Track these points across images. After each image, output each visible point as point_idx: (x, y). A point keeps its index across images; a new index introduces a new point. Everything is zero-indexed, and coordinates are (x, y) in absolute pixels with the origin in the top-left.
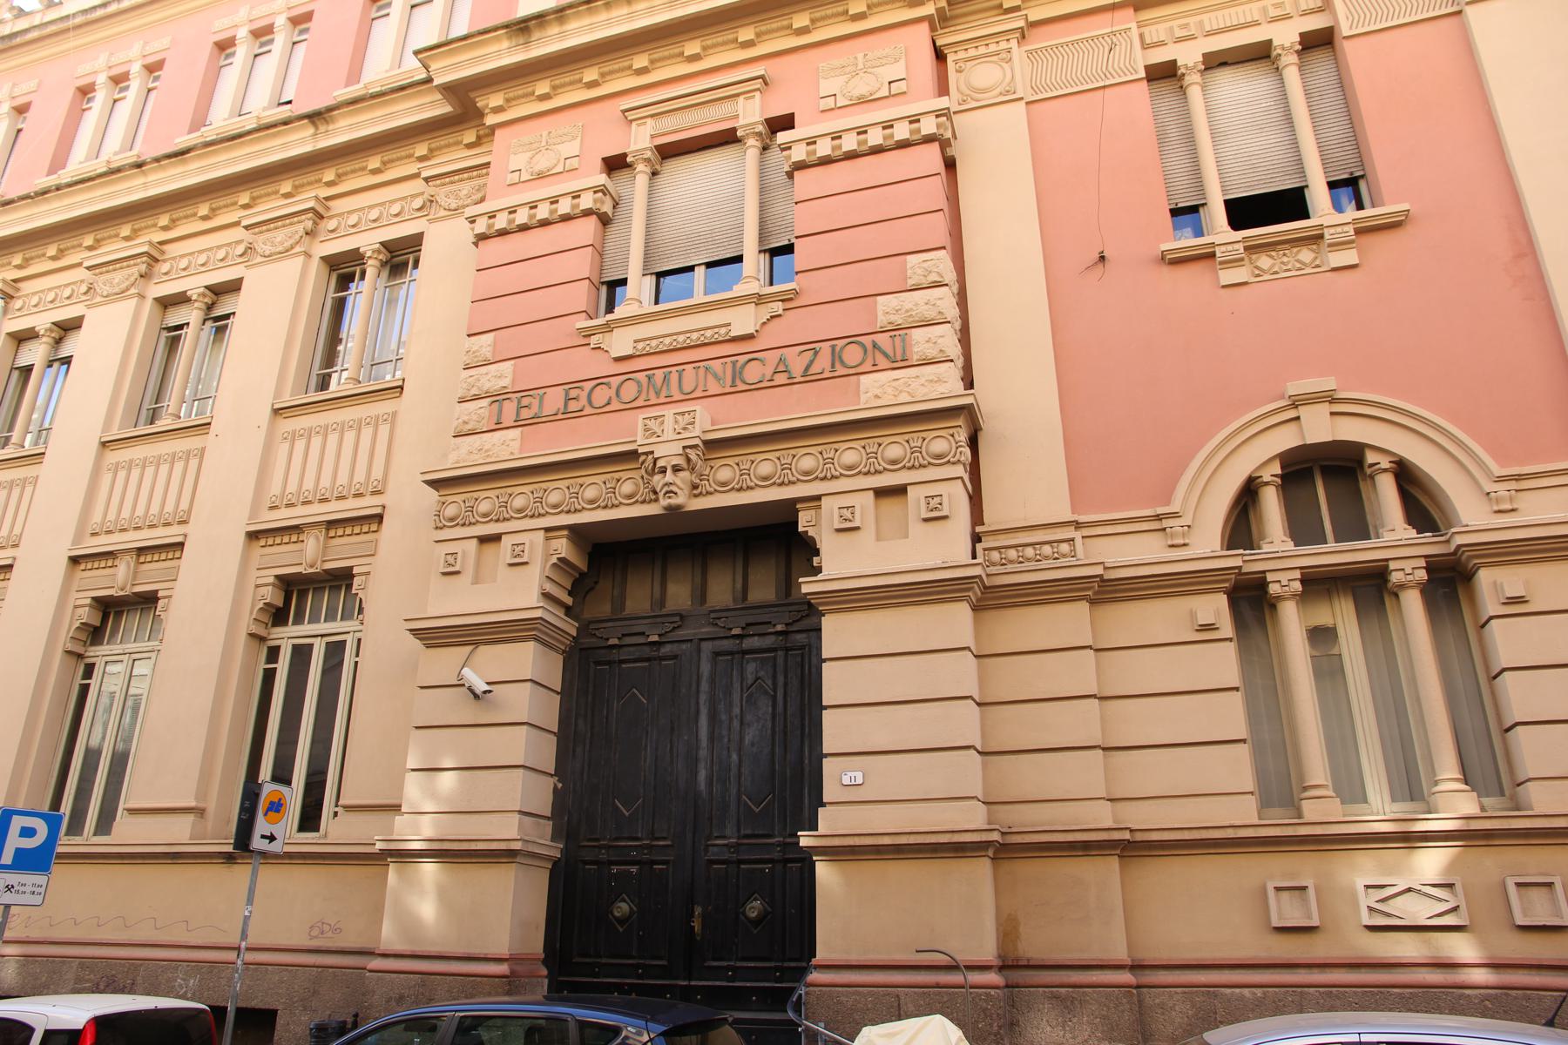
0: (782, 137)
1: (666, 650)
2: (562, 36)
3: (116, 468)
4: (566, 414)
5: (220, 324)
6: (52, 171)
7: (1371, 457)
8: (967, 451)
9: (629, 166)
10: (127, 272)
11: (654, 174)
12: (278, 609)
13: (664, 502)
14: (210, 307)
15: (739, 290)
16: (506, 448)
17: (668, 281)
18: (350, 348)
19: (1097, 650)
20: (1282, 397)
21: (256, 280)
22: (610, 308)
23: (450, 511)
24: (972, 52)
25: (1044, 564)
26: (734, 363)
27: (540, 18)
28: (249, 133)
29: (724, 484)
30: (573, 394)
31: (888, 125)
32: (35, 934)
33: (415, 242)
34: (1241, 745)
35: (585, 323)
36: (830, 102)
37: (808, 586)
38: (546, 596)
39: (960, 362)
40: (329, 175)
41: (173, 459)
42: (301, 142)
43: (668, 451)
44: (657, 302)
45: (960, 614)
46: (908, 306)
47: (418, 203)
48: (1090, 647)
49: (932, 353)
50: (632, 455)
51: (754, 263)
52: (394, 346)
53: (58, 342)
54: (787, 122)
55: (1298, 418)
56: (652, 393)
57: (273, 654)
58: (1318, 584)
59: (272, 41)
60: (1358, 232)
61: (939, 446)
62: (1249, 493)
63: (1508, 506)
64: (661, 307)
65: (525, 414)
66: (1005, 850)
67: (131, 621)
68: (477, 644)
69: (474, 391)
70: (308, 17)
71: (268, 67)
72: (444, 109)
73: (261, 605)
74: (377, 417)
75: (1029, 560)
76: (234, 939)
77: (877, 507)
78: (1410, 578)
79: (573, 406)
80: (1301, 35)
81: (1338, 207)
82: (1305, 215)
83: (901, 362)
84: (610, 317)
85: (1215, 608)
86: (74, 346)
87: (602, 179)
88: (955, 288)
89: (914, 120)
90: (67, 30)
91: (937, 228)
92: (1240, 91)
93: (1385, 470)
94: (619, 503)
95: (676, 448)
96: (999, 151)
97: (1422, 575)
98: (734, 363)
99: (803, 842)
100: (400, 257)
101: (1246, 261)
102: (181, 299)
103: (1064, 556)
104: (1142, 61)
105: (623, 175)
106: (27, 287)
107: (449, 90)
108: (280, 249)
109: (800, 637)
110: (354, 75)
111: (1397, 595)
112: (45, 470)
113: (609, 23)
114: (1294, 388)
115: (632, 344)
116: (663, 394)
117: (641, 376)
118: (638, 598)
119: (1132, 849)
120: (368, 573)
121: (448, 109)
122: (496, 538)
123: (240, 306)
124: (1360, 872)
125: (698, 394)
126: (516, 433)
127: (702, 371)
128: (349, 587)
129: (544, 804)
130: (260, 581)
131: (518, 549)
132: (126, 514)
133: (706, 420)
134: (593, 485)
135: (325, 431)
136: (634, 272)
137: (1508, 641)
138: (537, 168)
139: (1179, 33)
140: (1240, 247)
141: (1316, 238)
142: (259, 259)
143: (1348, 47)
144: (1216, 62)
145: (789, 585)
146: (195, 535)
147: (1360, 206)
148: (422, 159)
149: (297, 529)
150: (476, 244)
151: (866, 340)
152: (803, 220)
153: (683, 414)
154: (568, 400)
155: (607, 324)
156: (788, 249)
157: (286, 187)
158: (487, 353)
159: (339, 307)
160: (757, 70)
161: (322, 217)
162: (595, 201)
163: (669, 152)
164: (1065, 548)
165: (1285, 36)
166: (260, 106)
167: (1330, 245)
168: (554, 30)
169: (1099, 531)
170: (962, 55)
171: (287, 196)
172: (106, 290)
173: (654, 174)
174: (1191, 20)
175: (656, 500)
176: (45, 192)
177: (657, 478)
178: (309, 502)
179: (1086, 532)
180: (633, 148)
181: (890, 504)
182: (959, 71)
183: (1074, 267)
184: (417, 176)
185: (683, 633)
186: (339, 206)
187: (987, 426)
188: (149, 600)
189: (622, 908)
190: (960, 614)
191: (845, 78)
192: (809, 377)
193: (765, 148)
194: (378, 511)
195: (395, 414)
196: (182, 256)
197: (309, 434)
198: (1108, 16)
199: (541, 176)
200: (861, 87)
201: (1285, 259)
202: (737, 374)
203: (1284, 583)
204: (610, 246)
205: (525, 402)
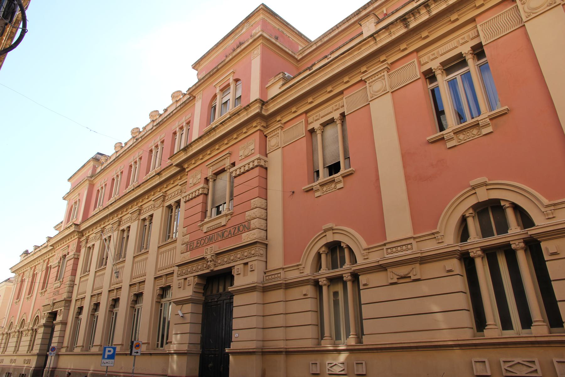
1: (219, 302)
2: (192, 150)
11: (215, 180)
32: (126, 371)
42: (157, 181)
50: (203, 258)
63: (441, 241)
66: (264, 353)
68: (183, 304)
72: (178, 169)
76: (131, 371)
79: (198, 245)
83: (249, 229)
93: (508, 207)
97: (522, 245)
99: (227, 351)
107: (177, 165)
113: (203, 143)
114: (473, 182)
119: (288, 353)
124: (329, 359)
126: (189, 253)
129: (199, 341)
133: (216, 247)
137: (366, 296)
139: (461, 41)
149: (161, 276)
160: (227, 152)
162: (258, 162)
164: (409, 246)
165: (466, 49)
182: (524, 4)
183: (290, 194)
189: (211, 365)
199: (194, 185)
201: (468, 134)
203: (323, 282)
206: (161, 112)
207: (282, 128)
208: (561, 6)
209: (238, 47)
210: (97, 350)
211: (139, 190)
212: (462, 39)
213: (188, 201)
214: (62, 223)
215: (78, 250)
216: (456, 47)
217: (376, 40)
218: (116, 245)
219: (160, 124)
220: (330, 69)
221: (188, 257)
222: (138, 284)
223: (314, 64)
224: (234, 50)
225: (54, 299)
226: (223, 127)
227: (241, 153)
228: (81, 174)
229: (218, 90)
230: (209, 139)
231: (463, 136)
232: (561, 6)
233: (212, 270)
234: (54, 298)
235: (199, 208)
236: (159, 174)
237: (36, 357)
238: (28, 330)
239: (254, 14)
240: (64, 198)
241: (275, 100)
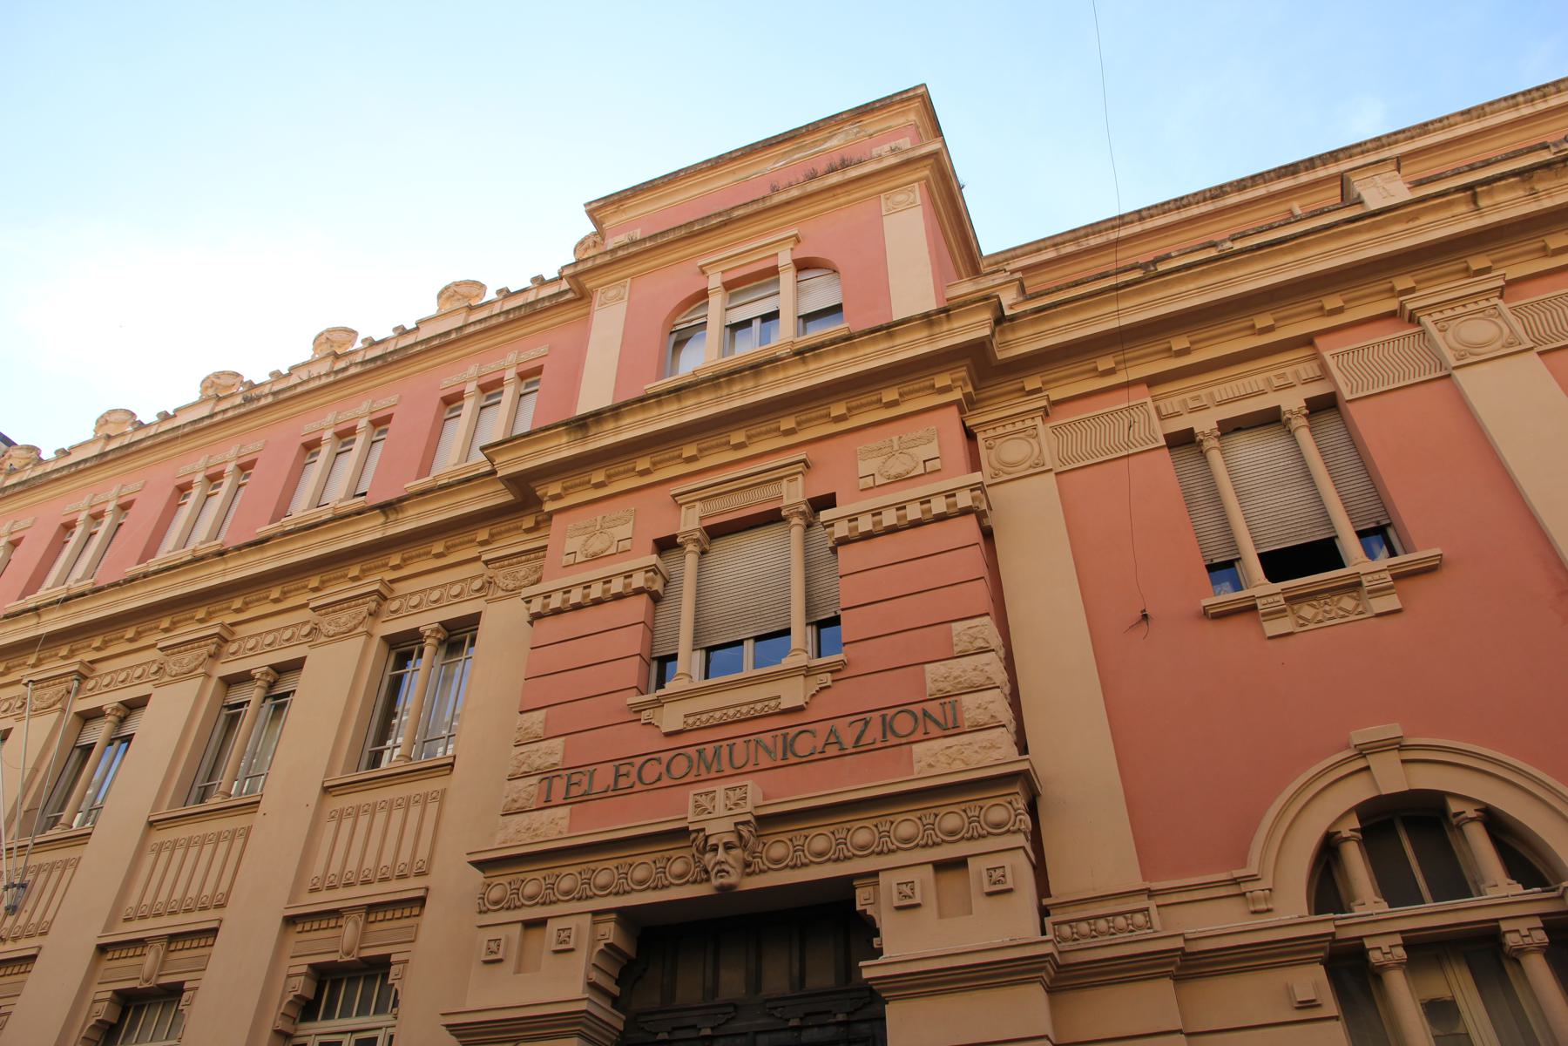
0: (825, 515)
2: (617, 430)
3: (160, 848)
4: (615, 790)
5: (279, 702)
6: (142, 560)
7: (1454, 807)
8: (1027, 818)
9: (680, 546)
10: (352, 611)
11: (703, 553)
12: (308, 1002)
13: (716, 882)
14: (271, 685)
15: (788, 662)
16: (555, 826)
17: (715, 655)
18: (405, 718)
19: (1188, 1035)
20: (1347, 747)
21: (19, 730)
22: (661, 684)
23: (495, 894)
24: (1000, 431)
25: (1120, 937)
26: (785, 736)
27: (598, 416)
28: (325, 522)
29: (777, 861)
30: (623, 770)
31: (925, 501)
33: (473, 621)
34: (1334, 1023)
36: (869, 482)
37: (870, 971)
38: (592, 986)
39: (1012, 727)
40: (395, 560)
41: (219, 838)
42: (371, 531)
43: (719, 828)
44: (707, 677)
45: (1034, 996)
46: (956, 673)
47: (477, 584)
48: (1180, 1031)
49: (983, 718)
50: (683, 833)
51: (801, 635)
52: (447, 718)
53: (122, 720)
54: (829, 501)
55: (1367, 768)
56: (703, 767)
58: (1425, 950)
60: (1395, 577)
61: (998, 815)
62: (1329, 850)
63: (1263, 907)
64: (711, 681)
65: (575, 791)
67: (152, 1017)
69: (525, 768)
70: (387, 419)
71: (348, 463)
73: (290, 997)
74: (426, 795)
75: (1102, 933)
77: (937, 881)
78: (1527, 940)
79: (623, 782)
80: (1306, 400)
81: (1371, 555)
82: (1338, 563)
83: (952, 728)
84: (660, 692)
85: (1312, 980)
86: (139, 725)
87: (653, 559)
88: (1002, 653)
89: (950, 494)
91: (980, 595)
92: (1255, 454)
93: (1472, 820)
94: (670, 884)
95: (728, 825)
96: (1035, 522)
97: (1541, 937)
98: (785, 736)
100: (458, 636)
101: (1289, 612)
102: (245, 678)
103: (1140, 928)
104: (1159, 431)
105: (673, 555)
106: (102, 668)
107: (512, 481)
108: (344, 629)
109: (864, 1027)
110: (425, 469)
111: (1518, 962)
112: (88, 853)
113: (660, 418)
114: (1359, 737)
115: (682, 719)
116: (714, 768)
117: (692, 751)
118: (689, 987)
120: (406, 961)
121: (510, 497)
122: (541, 923)
123: (303, 686)
125: (749, 768)
126: (564, 811)
127: (752, 744)
128: (386, 976)
130: (292, 971)
131: (563, 935)
132: (163, 897)
133: (757, 794)
134: (642, 866)
135: (373, 810)
136: (684, 646)
138: (591, 551)
139: (1192, 405)
140: (1281, 598)
141: (1354, 586)
142: (323, 639)
143: (1352, 409)
144: (1229, 428)
145: (848, 970)
146: (231, 919)
147: (1393, 553)
148: (483, 543)
149: (336, 913)
150: (531, 623)
151: (916, 708)
152: (848, 592)
153: (734, 789)
154: (618, 776)
155: (658, 699)
156: (835, 621)
157: (354, 571)
158: (539, 730)
159: (396, 684)
161: (385, 599)
162: (647, 580)
163: (717, 532)
165: (1292, 402)
166: (337, 496)
167: (1370, 592)
168: (611, 425)
169: (1175, 898)
170: (991, 433)
171: (354, 579)
172: (176, 669)
173: (703, 553)
174: (1202, 393)
175: (708, 880)
177: (708, 856)
178: (352, 884)
179: (1161, 900)
180: (683, 529)
181: (951, 879)
182: (989, 448)
183: (1121, 628)
184: (477, 559)
185: (738, 1026)
186: (402, 588)
187: (1045, 790)
188: (171, 994)
190: (1034, 996)
191: (882, 459)
192: (860, 748)
193: (809, 526)
194: (421, 893)
195: (444, 791)
196: (286, 628)
197: (356, 813)
198: (1124, 393)
200: (898, 466)
202: (788, 747)
203: (1385, 950)
204: (661, 622)
205: (575, 779)
206: (47, 454)
207: (1046, 414)
208: (1052, 474)
209: (832, 170)
212: (1279, 377)
216: (1262, 393)
217: (1475, 202)
218: (35, 770)
219: (127, 452)
220: (1289, 258)
223: (1168, 257)
224: (813, 176)
226: (801, 369)
229: (715, 281)
230: (718, 401)
231: (1313, 611)
232: (1052, 474)
233: (725, 890)
239: (892, 104)
241: (1047, 319)
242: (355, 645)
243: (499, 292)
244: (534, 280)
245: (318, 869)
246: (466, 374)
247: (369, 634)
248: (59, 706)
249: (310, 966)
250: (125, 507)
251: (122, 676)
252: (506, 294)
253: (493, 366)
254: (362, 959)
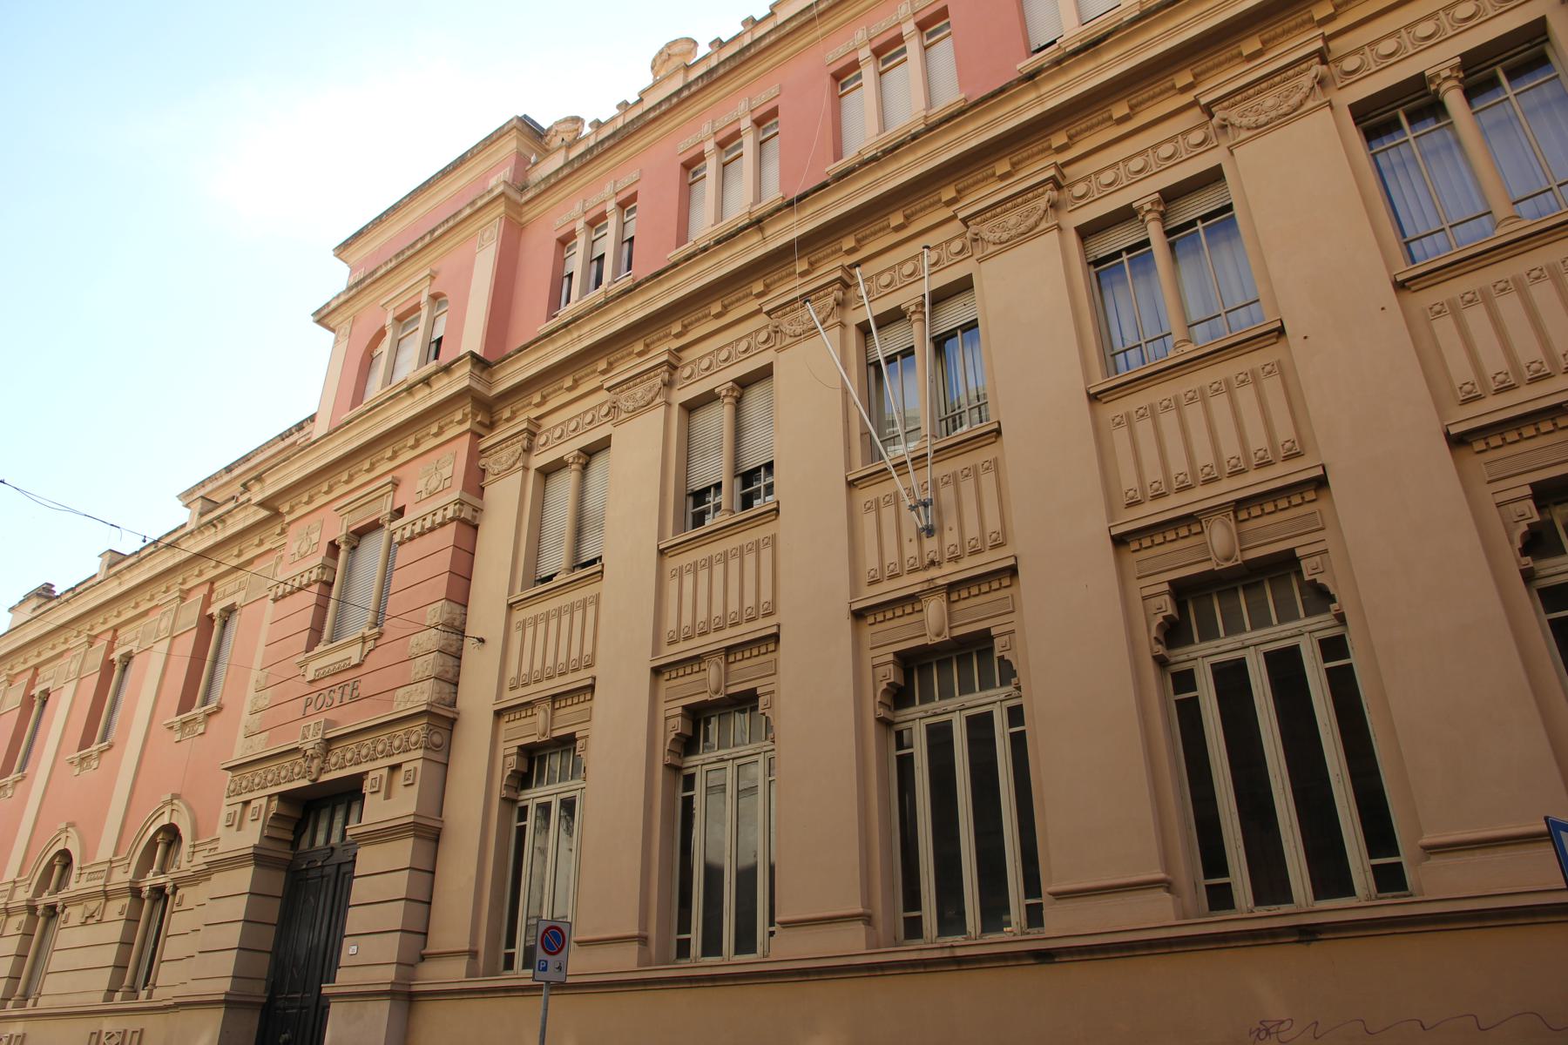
10: (647, 385)
11: (354, 548)
21: (787, 365)
35: (301, 658)
40: (848, 243)
42: (753, 249)
47: (763, 336)
50: (296, 750)
57: (523, 813)
59: (741, 145)
72: (264, 513)
90: (812, 20)
106: (688, 355)
107: (262, 504)
110: (682, 238)
120: (1013, 632)
130: (876, 661)
132: (526, 669)
142: (624, 415)
146: (789, 620)
148: (760, 295)
149: (697, 659)
161: (675, 368)
171: (1003, 177)
176: (675, 265)
184: (759, 311)
196: (721, 349)
199: (431, 494)
210: (633, 965)
211: (795, 218)
213: (283, 597)
214: (312, 418)
215: (476, 481)
221: (260, 747)
222: (547, 706)
225: (330, 724)
227: (420, 486)
228: (421, 209)
229: (389, 320)
234: (330, 715)
235: (307, 618)
236: (758, 224)
237: (218, 1015)
238: (107, 895)
240: (323, 317)
242: (656, 417)
243: (711, 44)
244: (744, 23)
245: (671, 624)
246: (697, 130)
247: (843, 325)
248: (519, 464)
249: (896, 654)
250: (626, 205)
251: (573, 425)
252: (718, 44)
253: (726, 119)
254: (954, 639)
